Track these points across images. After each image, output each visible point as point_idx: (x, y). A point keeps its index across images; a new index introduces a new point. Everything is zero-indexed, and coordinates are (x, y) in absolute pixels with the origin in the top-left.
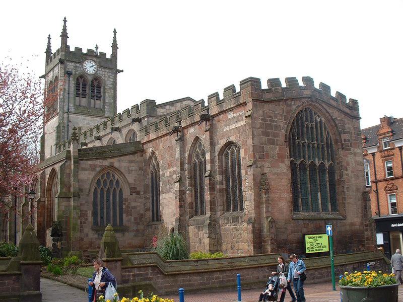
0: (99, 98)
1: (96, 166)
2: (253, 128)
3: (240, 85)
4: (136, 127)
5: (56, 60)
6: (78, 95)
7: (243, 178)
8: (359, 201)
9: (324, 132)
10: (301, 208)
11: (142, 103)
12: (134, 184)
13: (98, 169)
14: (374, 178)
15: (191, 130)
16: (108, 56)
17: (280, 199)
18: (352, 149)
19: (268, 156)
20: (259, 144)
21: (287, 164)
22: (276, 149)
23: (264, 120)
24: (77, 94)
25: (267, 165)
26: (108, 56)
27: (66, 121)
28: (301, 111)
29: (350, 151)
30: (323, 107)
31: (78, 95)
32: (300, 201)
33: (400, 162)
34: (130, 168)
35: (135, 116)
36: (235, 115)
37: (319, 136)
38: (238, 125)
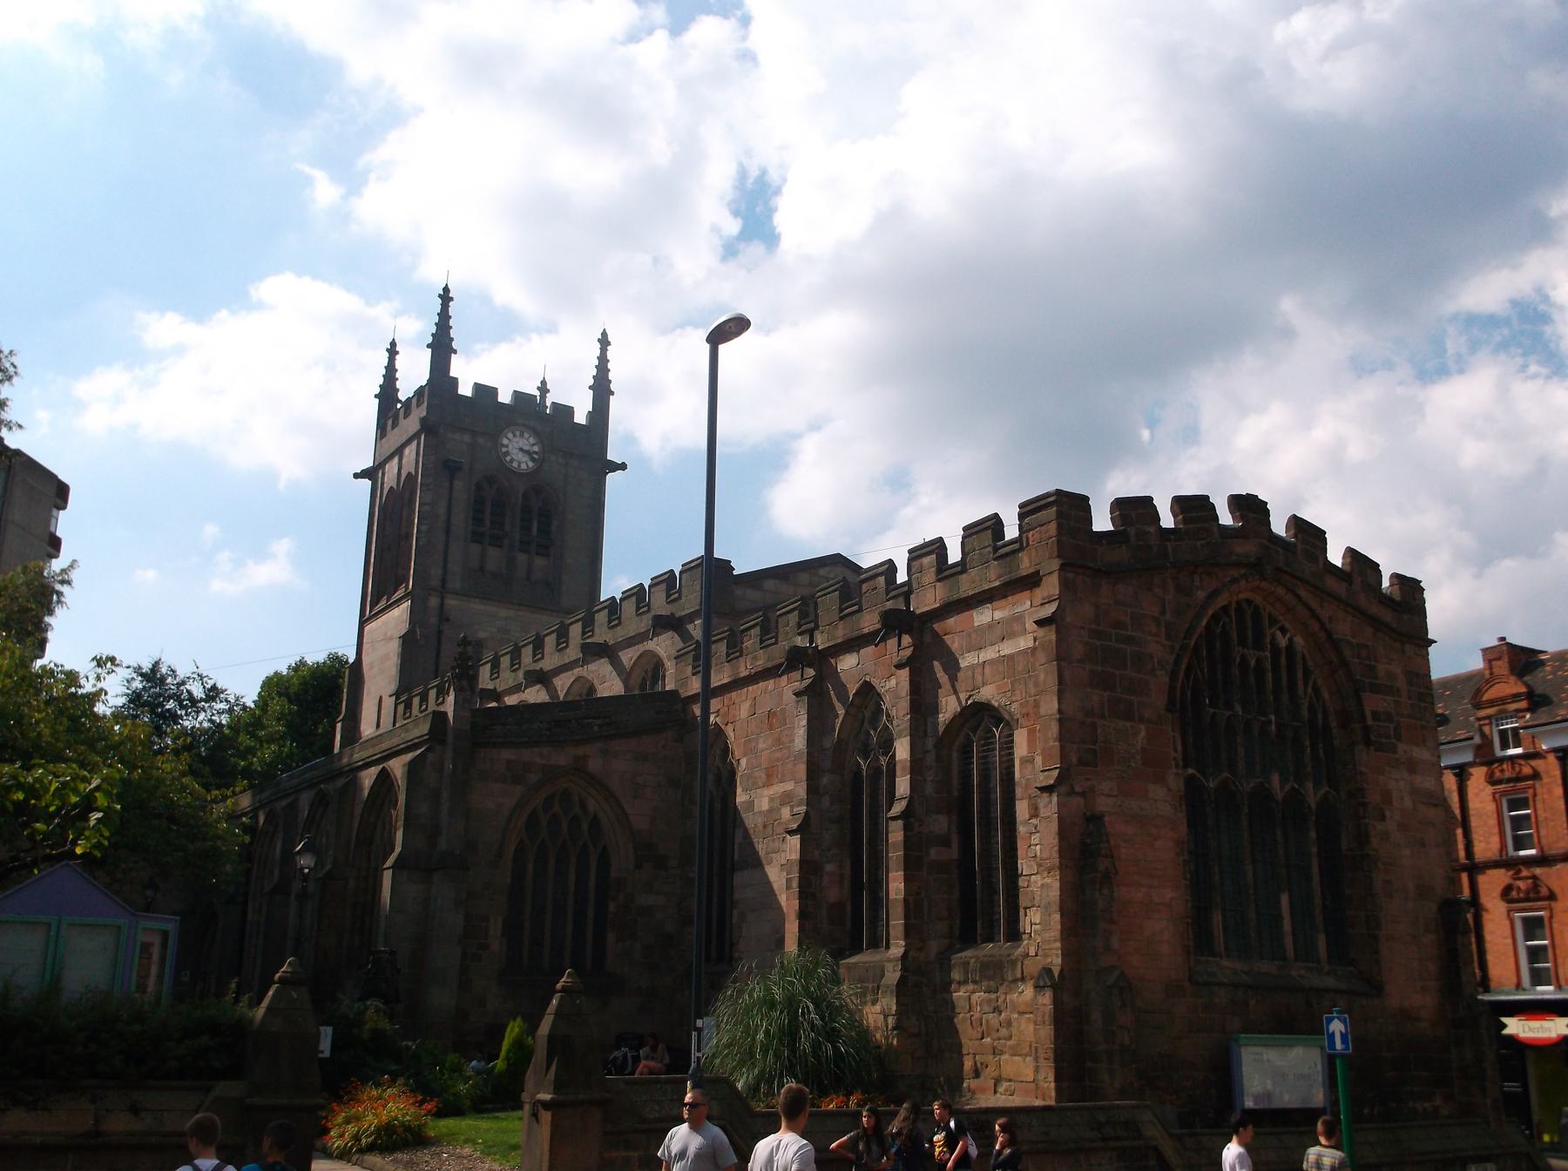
0: (544, 550)
2: (1061, 657)
3: (1021, 516)
4: (664, 646)
5: (411, 424)
6: (477, 537)
7: (1022, 829)
13: (533, 778)
15: (847, 663)
16: (580, 418)
18: (1401, 747)
26: (580, 418)
27: (433, 620)
28: (1225, 609)
30: (1298, 597)
31: (477, 537)
32: (1217, 918)
35: (660, 605)
36: (998, 615)
37: (1285, 698)
38: (1007, 648)
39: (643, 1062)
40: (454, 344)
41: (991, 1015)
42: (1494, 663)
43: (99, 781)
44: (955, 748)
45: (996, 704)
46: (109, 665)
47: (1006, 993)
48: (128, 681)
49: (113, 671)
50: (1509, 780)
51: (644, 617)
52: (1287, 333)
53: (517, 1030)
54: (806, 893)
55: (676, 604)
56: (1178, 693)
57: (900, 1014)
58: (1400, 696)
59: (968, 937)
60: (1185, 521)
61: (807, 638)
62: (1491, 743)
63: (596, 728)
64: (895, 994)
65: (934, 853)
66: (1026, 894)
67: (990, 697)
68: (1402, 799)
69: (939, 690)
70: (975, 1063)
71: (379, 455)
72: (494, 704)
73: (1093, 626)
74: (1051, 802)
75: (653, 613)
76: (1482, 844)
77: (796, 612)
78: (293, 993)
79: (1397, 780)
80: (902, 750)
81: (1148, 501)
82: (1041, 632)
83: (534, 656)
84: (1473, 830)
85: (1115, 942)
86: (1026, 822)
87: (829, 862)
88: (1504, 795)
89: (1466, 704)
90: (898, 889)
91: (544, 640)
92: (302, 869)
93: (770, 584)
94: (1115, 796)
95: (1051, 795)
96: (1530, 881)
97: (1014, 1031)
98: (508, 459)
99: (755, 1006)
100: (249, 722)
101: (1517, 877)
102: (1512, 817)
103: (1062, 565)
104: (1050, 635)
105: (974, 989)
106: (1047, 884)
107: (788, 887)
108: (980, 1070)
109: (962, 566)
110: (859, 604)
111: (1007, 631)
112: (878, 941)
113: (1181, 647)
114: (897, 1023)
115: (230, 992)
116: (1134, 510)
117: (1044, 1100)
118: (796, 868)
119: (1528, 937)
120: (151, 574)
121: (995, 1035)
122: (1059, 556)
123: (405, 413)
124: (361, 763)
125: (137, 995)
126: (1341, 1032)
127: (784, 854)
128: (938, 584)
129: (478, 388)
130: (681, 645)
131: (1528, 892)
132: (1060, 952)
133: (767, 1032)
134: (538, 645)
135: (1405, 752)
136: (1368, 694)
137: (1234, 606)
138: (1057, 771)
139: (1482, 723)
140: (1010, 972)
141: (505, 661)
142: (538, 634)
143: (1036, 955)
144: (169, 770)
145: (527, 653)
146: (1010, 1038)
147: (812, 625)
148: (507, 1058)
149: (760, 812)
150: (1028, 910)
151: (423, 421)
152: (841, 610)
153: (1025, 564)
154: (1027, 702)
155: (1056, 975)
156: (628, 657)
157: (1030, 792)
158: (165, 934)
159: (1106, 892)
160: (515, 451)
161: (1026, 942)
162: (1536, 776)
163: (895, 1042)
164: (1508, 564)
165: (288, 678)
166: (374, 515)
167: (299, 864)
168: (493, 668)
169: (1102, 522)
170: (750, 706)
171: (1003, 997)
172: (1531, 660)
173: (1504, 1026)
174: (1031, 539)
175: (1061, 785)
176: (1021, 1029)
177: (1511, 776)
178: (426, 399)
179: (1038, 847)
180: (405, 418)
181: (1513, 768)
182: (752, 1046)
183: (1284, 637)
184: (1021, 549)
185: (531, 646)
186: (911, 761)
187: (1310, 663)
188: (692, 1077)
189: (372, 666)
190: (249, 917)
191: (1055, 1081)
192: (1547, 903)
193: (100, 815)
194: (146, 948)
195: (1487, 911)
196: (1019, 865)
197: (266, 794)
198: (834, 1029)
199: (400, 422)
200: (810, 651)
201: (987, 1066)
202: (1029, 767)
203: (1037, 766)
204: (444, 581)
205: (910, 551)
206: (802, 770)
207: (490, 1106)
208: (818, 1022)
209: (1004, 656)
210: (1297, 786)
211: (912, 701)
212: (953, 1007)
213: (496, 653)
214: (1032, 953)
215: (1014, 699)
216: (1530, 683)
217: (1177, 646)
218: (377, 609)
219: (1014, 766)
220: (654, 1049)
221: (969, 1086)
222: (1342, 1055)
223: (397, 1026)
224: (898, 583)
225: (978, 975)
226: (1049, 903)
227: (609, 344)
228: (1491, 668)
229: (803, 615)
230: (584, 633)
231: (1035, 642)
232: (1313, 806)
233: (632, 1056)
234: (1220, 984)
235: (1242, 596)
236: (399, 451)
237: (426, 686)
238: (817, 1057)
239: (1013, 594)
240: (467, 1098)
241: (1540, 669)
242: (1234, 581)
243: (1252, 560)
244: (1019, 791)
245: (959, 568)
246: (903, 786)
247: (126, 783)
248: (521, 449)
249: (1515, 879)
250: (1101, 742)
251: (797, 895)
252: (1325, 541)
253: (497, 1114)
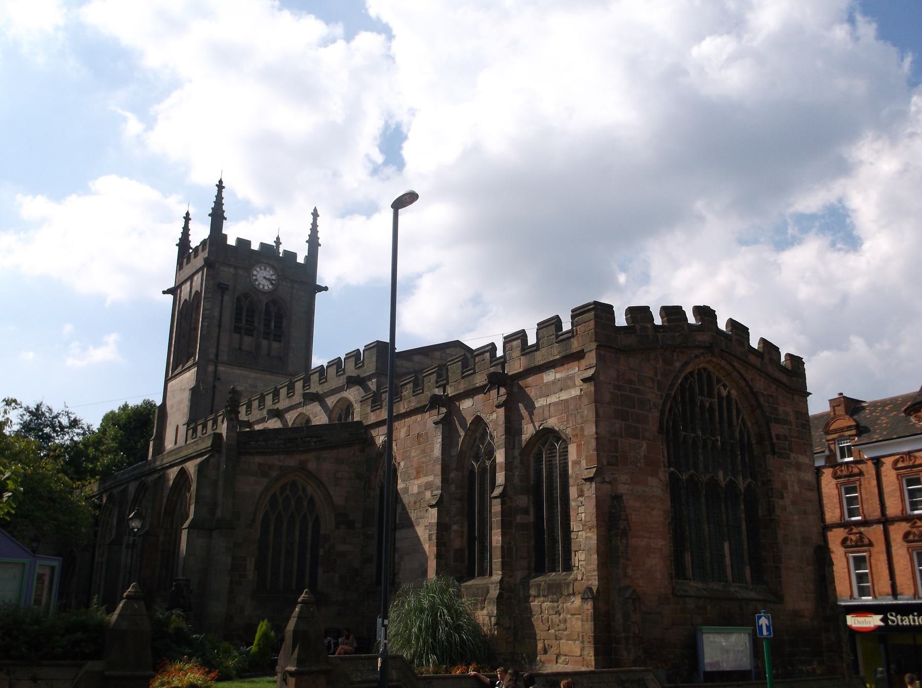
0: (278, 338)
2: (597, 400)
3: (573, 317)
4: (353, 394)
5: (198, 262)
6: (237, 330)
7: (573, 504)
9: (735, 418)
10: (689, 573)
11: (368, 348)
13: (274, 474)
15: (466, 405)
16: (301, 259)
18: (792, 455)
24: (236, 327)
25: (624, 478)
26: (301, 259)
27: (211, 379)
28: (691, 373)
30: (733, 366)
31: (237, 330)
32: (688, 557)
33: (876, 489)
35: (351, 370)
36: (558, 376)
37: (726, 426)
38: (564, 396)
39: (341, 646)
40: (225, 215)
41: (554, 616)
42: (836, 408)
43: (10, 473)
44: (532, 455)
45: (557, 429)
46: (13, 404)
47: (563, 603)
48: (21, 416)
49: (16, 408)
50: (845, 476)
51: (342, 377)
52: (701, 219)
53: (264, 627)
54: (441, 543)
55: (361, 369)
56: (665, 421)
57: (499, 616)
58: (791, 425)
59: (540, 569)
60: (669, 321)
61: (442, 389)
62: (835, 455)
63: (313, 444)
64: (496, 604)
65: (519, 518)
66: (576, 543)
67: (553, 425)
68: (793, 486)
69: (523, 421)
70: (545, 645)
71: (179, 280)
72: (248, 429)
73: (616, 383)
74: (591, 487)
75: (347, 375)
76: (830, 514)
77: (435, 375)
78: (135, 605)
79: (790, 475)
80: (500, 457)
81: (646, 309)
82: (585, 386)
83: (273, 400)
84: (825, 505)
85: (630, 571)
86: (575, 500)
87: (455, 524)
88: (843, 485)
89: (821, 431)
90: (498, 540)
91: (279, 391)
92: (133, 528)
93: (417, 358)
94: (629, 484)
95: (591, 483)
96: (858, 535)
97: (568, 625)
98: (257, 283)
99: (411, 611)
100: (95, 441)
101: (913, 526)
102: (847, 498)
103: (597, 345)
104: (590, 387)
105: (543, 601)
106: (589, 537)
107: (430, 539)
108: (547, 649)
109: (537, 347)
110: (474, 369)
111: (564, 385)
112: (485, 571)
113: (667, 395)
114: (496, 621)
115: (93, 604)
116: (639, 314)
117: (588, 667)
118: (435, 528)
119: (857, 568)
120: (31, 355)
121: (557, 628)
122: (596, 341)
123: (195, 255)
124: (168, 465)
125: (36, 607)
126: (766, 625)
127: (427, 520)
128: (522, 357)
129: (239, 240)
130: (364, 394)
131: (856, 542)
132: (597, 578)
133: (420, 628)
134: (276, 394)
135: (795, 458)
136: (773, 424)
137: (696, 371)
138: (595, 469)
139: (829, 443)
140: (566, 590)
141: (255, 404)
142: (276, 388)
143: (582, 580)
144: (50, 469)
145: (269, 399)
146: (566, 629)
147: (445, 382)
148: (258, 645)
149: (413, 494)
150: (577, 553)
151: (206, 260)
152: (463, 373)
153: (575, 346)
154: (576, 427)
155: (595, 592)
156: (331, 401)
157: (578, 482)
158: (53, 569)
159: (624, 541)
160: (261, 279)
161: (576, 572)
162: (861, 474)
163: (496, 633)
164: (825, 354)
165: (119, 415)
166: (175, 316)
167: (131, 525)
168: (247, 408)
169: (621, 320)
170: (407, 430)
171: (561, 605)
172: (857, 406)
173: (882, 620)
174: (579, 331)
175: (598, 477)
176: (573, 624)
177: (847, 474)
178: (207, 246)
179: (583, 515)
180: (202, 251)
181: (848, 469)
182: (410, 635)
183: (725, 390)
184: (573, 336)
185: (272, 394)
186: (506, 463)
187: (740, 406)
188: (381, 656)
189: (172, 407)
190: (96, 558)
191: (595, 656)
192: (868, 548)
193: (10, 494)
194: (40, 577)
195: (833, 552)
196: (571, 526)
197: (108, 484)
198: (459, 625)
199: (191, 260)
200: (443, 397)
201: (552, 647)
202: (578, 467)
203: (582, 466)
204: (217, 356)
205: (538, 325)
206: (438, 468)
207: (248, 674)
208: (450, 621)
209: (562, 400)
210: (733, 478)
211: (506, 427)
212: (531, 612)
213: (250, 399)
214: (579, 578)
215: (568, 426)
216: (857, 419)
217: (664, 395)
218: (176, 372)
219: (568, 466)
220: (347, 638)
221: (541, 659)
222: (767, 639)
223: (190, 626)
224: (497, 356)
225: (546, 591)
226: (590, 548)
227: (318, 216)
228: (834, 411)
229: (439, 376)
230: (304, 387)
231: (581, 392)
232: (742, 490)
233: (334, 643)
234: (690, 596)
235: (701, 366)
236: (191, 278)
237: (206, 419)
238: (448, 640)
239: (568, 363)
240: (234, 670)
241: (863, 411)
242: (697, 356)
243: (707, 344)
244: (571, 481)
245: (535, 348)
246: (500, 478)
247: (25, 475)
248: (265, 278)
249: (912, 528)
250: (621, 452)
251: (435, 544)
252: (748, 334)
253: (253, 679)
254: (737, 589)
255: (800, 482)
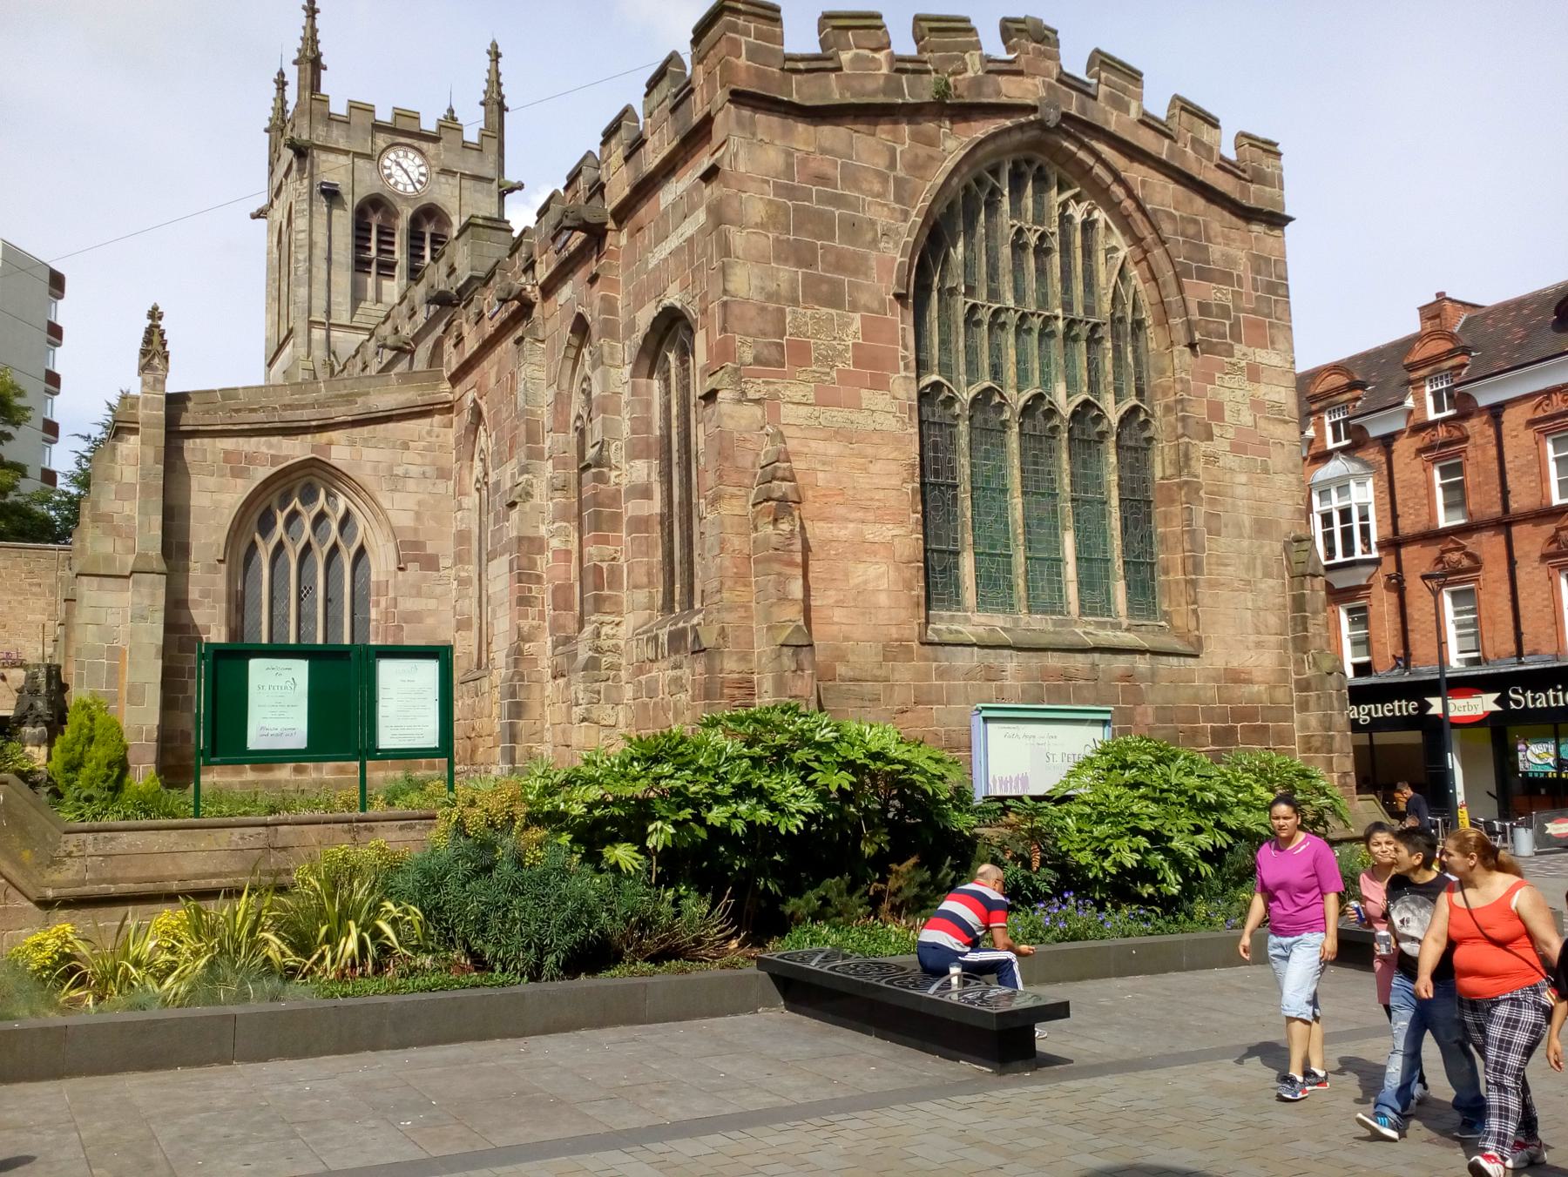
1: (251, 459)
8: (1267, 575)
10: (969, 595)
12: (416, 530)
14: (1388, 531)
17: (861, 549)
18: (1239, 349)
19: (801, 353)
20: (756, 297)
21: (902, 394)
22: (848, 324)
23: (789, 191)
25: (796, 392)
29: (1232, 356)
34: (399, 471)
98: (392, 181)
173: (1497, 702)
254: (1090, 629)
255: (1257, 405)
